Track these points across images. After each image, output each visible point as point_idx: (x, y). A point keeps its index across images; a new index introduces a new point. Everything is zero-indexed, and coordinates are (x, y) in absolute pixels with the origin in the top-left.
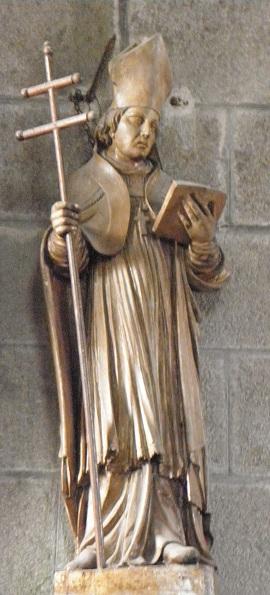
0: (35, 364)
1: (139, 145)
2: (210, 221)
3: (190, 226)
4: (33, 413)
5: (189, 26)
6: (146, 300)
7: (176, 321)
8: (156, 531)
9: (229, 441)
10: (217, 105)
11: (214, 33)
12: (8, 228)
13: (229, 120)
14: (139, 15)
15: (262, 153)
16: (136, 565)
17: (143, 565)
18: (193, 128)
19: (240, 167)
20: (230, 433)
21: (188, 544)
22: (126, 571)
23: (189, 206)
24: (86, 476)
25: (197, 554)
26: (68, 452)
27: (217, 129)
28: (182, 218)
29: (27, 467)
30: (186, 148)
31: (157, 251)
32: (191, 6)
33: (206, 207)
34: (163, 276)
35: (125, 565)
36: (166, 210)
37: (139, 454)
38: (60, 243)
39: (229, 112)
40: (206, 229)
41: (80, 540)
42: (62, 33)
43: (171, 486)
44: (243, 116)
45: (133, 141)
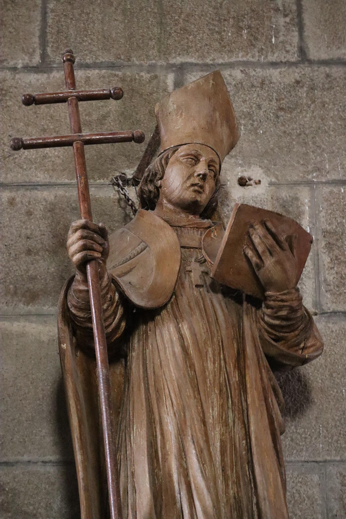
0: (56, 486)
1: (192, 188)
2: (289, 259)
5: (259, 107)
7: (245, 391)
10: (296, 184)
11: (291, 112)
12: (27, 324)
13: (312, 197)
27: (298, 207)
28: (250, 253)
32: (262, 88)
39: (312, 189)
42: (104, 117)
44: (331, 192)
45: (185, 182)
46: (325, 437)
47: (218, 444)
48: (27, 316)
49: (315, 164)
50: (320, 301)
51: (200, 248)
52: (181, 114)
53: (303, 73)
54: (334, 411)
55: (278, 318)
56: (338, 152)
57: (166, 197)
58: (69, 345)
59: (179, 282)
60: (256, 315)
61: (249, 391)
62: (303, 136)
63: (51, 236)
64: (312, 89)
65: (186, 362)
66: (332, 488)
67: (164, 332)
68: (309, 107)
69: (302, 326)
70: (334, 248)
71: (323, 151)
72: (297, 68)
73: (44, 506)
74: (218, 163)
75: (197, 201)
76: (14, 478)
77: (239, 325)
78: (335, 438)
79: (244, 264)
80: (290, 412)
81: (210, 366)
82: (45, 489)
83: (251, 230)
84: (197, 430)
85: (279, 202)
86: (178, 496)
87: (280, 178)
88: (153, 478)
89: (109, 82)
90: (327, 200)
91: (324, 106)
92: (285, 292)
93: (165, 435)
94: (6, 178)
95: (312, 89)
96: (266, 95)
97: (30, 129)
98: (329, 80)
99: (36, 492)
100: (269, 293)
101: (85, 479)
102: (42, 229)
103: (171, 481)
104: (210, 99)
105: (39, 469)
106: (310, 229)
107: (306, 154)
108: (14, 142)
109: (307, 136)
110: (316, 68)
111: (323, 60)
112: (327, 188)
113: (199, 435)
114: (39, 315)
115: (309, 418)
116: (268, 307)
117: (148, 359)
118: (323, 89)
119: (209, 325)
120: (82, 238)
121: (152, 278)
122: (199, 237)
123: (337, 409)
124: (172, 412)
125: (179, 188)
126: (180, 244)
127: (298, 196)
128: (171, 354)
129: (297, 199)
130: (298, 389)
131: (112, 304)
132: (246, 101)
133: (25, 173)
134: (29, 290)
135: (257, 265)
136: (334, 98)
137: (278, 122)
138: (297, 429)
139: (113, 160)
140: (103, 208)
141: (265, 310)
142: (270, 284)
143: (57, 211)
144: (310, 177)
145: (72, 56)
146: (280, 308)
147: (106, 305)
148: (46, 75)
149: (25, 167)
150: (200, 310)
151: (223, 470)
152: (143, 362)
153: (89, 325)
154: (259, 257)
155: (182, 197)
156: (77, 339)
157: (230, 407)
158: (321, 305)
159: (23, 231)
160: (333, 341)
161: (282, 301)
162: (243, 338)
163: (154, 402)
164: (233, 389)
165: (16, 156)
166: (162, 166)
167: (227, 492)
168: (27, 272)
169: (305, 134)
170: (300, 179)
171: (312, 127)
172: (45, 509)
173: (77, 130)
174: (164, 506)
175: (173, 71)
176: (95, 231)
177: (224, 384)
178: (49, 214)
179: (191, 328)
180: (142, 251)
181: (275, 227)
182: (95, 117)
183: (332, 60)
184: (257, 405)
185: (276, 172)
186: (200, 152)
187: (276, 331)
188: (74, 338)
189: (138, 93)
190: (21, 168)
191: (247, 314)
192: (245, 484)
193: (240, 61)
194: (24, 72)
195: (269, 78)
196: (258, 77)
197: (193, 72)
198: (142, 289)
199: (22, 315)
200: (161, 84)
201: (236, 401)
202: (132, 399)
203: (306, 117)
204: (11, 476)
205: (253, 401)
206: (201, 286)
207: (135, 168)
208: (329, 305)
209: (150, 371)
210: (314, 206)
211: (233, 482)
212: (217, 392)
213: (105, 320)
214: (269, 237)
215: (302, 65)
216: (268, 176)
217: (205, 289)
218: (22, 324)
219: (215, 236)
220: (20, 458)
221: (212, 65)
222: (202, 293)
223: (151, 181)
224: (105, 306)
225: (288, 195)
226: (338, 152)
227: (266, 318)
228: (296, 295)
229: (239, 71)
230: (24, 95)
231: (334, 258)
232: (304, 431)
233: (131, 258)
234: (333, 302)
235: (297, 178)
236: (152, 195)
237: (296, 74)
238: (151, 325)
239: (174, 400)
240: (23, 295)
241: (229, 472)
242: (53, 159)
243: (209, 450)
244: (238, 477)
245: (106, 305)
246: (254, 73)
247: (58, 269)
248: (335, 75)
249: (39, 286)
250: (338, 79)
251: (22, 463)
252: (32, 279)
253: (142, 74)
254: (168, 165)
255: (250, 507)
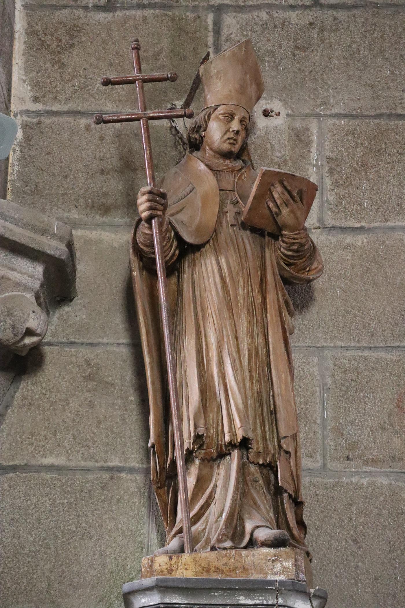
0: (128, 362)
1: (228, 141)
2: (299, 209)
3: (279, 213)
4: (126, 410)
5: (280, 46)
6: (234, 283)
7: (266, 309)
8: (246, 516)
9: (324, 437)
10: (307, 116)
11: (305, 51)
12: (103, 233)
13: (320, 128)
14: (232, 36)
15: (353, 159)
16: (225, 549)
17: (231, 548)
18: (285, 137)
19: (331, 171)
20: (324, 428)
21: (278, 527)
22: (215, 553)
23: (277, 192)
24: (174, 462)
25: (287, 536)
26: (155, 440)
28: (271, 205)
29: (121, 462)
30: (279, 155)
31: (246, 242)
33: (295, 194)
34: (252, 263)
35: (213, 549)
36: (255, 198)
37: (227, 439)
38: (147, 231)
39: (319, 121)
40: (296, 218)
41: (171, 529)
42: (159, 53)
43: (261, 473)
44: (334, 124)
45: (223, 136)
46: (323, 328)
47: (246, 352)
48: (102, 226)
49: (322, 99)
50: (323, 218)
51: (234, 191)
52: (220, 78)
53: (315, 16)
54: (330, 308)
55: (291, 250)
56: (341, 88)
57: (209, 146)
58: (138, 273)
59: (219, 222)
60: (275, 246)
61: (268, 311)
62: (314, 72)
63: (119, 159)
64: (322, 30)
65: (224, 289)
66: (327, 367)
67: (207, 263)
68: (319, 47)
69: (309, 254)
70: (335, 173)
71: (329, 87)
72: (311, 11)
73: (120, 378)
74: (248, 119)
75: (232, 151)
76: (97, 356)
77: (262, 256)
78: (331, 329)
79: (267, 211)
80: (298, 308)
81: (241, 292)
82: (120, 365)
83: (272, 188)
84: (232, 345)
85: (293, 132)
86: (218, 392)
87: (295, 110)
88: (201, 378)
89: (162, 21)
90: (330, 131)
91: (331, 46)
92: (296, 232)
93: (209, 345)
94: (83, 107)
95: (322, 30)
96: (285, 35)
97: (100, 62)
98: (336, 22)
99: (113, 367)
100: (284, 232)
101: (152, 376)
102: (112, 152)
103: (213, 381)
104: (242, 64)
105: (115, 349)
106: (317, 155)
107: (316, 89)
108: (97, 119)
109: (317, 72)
110: (326, 12)
111: (331, 4)
112: (331, 120)
113: (233, 349)
114: (111, 225)
115: (312, 312)
116: (284, 242)
117: (195, 283)
118: (331, 31)
119: (240, 259)
120: (149, 200)
121: (199, 218)
122: (233, 179)
123: (333, 306)
124: (213, 328)
125: (219, 141)
126: (219, 187)
127: (308, 127)
128: (213, 282)
129: (308, 129)
130: (305, 289)
131: (169, 241)
132: (270, 40)
133: (98, 102)
134: (103, 204)
135: (276, 213)
136: (340, 39)
137: (295, 60)
138: (303, 321)
139: (165, 92)
140: (159, 135)
141: (281, 243)
142: (285, 226)
143: (123, 136)
144: (318, 110)
145: (138, 45)
146: (293, 244)
147: (165, 243)
148: (111, 14)
149: (97, 98)
150: (234, 245)
151: (249, 372)
152: (192, 285)
153: (153, 256)
154: (278, 207)
155: (220, 148)
156: (143, 263)
157: (255, 322)
158: (324, 221)
159: (97, 153)
160: (332, 251)
161: (294, 239)
162: (265, 267)
163: (201, 318)
164: (257, 310)
165: (90, 87)
166: (206, 121)
167: (252, 388)
168: (102, 189)
169: (315, 71)
170: (311, 112)
171: (321, 65)
172: (121, 380)
173: (143, 109)
174: (208, 400)
175: (213, 12)
176: (158, 195)
177: (251, 305)
178: (116, 139)
179: (228, 262)
180: (191, 192)
181: (290, 185)
182: (151, 53)
183: (338, 4)
184: (274, 321)
185: (292, 105)
186: (235, 111)
187: (289, 259)
188: (141, 263)
189: (184, 31)
190: (94, 98)
191: (268, 247)
192: (265, 382)
193: (266, 4)
194: (94, 11)
195: (288, 20)
196: (280, 18)
197: (228, 12)
198: (191, 227)
199: (99, 226)
200: (203, 23)
201: (259, 318)
202: (184, 313)
203: (317, 56)
204: (95, 354)
205: (272, 318)
206: (235, 225)
207: (184, 100)
208: (329, 221)
209: (197, 293)
210: (321, 135)
211: (257, 380)
212: (246, 312)
213: (165, 253)
214: (286, 193)
215: (315, 9)
216: (286, 108)
217: (237, 227)
218: (99, 232)
219: (245, 177)
220: (100, 340)
221: (243, 6)
222: (236, 231)
223: (197, 132)
224: (164, 244)
225: (301, 126)
226: (341, 88)
227: (282, 249)
228: (304, 234)
229: (265, 13)
230: (103, 79)
231: (335, 181)
232: (308, 323)
233: (182, 199)
234: (333, 219)
235: (308, 111)
236: (198, 142)
237: (310, 17)
238: (198, 255)
239: (215, 320)
240: (99, 209)
241: (254, 374)
242: (119, 91)
243: (240, 358)
244: (260, 377)
245: (165, 243)
246: (277, 15)
247: (124, 187)
248: (341, 18)
249: (110, 201)
250: (343, 22)
251: (103, 344)
252: (106, 195)
253: (188, 14)
254: (211, 120)
255: (268, 399)
